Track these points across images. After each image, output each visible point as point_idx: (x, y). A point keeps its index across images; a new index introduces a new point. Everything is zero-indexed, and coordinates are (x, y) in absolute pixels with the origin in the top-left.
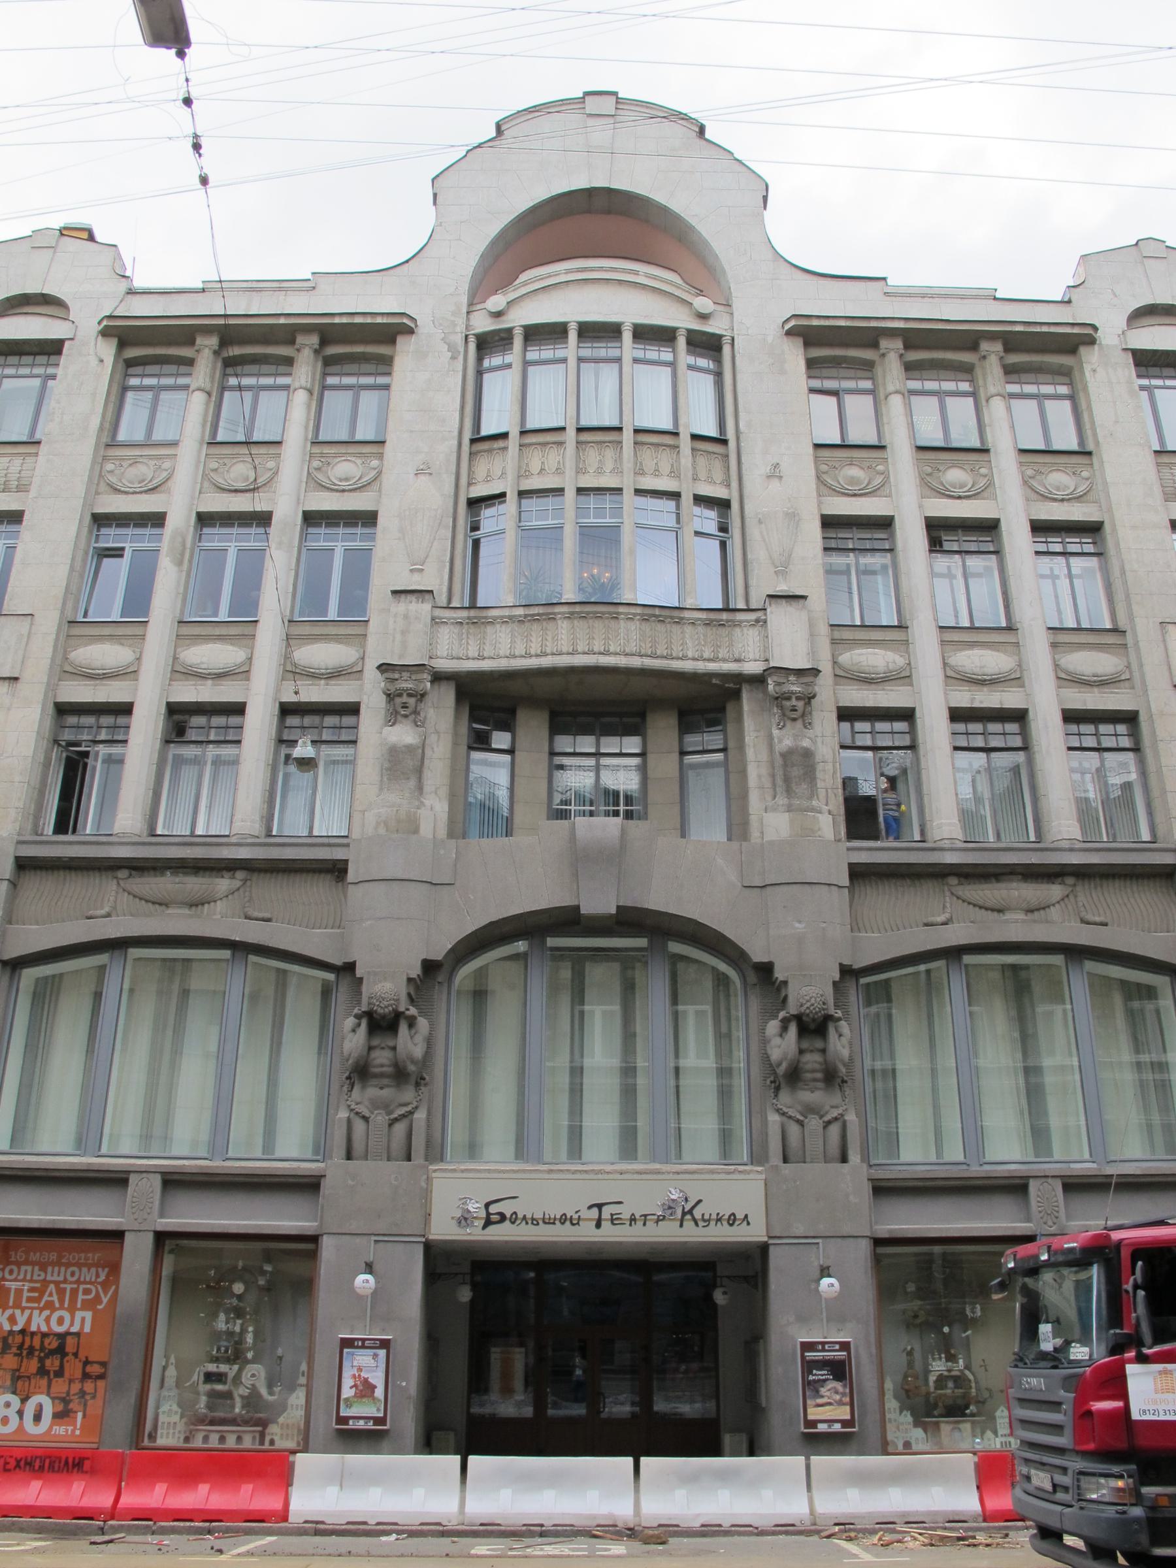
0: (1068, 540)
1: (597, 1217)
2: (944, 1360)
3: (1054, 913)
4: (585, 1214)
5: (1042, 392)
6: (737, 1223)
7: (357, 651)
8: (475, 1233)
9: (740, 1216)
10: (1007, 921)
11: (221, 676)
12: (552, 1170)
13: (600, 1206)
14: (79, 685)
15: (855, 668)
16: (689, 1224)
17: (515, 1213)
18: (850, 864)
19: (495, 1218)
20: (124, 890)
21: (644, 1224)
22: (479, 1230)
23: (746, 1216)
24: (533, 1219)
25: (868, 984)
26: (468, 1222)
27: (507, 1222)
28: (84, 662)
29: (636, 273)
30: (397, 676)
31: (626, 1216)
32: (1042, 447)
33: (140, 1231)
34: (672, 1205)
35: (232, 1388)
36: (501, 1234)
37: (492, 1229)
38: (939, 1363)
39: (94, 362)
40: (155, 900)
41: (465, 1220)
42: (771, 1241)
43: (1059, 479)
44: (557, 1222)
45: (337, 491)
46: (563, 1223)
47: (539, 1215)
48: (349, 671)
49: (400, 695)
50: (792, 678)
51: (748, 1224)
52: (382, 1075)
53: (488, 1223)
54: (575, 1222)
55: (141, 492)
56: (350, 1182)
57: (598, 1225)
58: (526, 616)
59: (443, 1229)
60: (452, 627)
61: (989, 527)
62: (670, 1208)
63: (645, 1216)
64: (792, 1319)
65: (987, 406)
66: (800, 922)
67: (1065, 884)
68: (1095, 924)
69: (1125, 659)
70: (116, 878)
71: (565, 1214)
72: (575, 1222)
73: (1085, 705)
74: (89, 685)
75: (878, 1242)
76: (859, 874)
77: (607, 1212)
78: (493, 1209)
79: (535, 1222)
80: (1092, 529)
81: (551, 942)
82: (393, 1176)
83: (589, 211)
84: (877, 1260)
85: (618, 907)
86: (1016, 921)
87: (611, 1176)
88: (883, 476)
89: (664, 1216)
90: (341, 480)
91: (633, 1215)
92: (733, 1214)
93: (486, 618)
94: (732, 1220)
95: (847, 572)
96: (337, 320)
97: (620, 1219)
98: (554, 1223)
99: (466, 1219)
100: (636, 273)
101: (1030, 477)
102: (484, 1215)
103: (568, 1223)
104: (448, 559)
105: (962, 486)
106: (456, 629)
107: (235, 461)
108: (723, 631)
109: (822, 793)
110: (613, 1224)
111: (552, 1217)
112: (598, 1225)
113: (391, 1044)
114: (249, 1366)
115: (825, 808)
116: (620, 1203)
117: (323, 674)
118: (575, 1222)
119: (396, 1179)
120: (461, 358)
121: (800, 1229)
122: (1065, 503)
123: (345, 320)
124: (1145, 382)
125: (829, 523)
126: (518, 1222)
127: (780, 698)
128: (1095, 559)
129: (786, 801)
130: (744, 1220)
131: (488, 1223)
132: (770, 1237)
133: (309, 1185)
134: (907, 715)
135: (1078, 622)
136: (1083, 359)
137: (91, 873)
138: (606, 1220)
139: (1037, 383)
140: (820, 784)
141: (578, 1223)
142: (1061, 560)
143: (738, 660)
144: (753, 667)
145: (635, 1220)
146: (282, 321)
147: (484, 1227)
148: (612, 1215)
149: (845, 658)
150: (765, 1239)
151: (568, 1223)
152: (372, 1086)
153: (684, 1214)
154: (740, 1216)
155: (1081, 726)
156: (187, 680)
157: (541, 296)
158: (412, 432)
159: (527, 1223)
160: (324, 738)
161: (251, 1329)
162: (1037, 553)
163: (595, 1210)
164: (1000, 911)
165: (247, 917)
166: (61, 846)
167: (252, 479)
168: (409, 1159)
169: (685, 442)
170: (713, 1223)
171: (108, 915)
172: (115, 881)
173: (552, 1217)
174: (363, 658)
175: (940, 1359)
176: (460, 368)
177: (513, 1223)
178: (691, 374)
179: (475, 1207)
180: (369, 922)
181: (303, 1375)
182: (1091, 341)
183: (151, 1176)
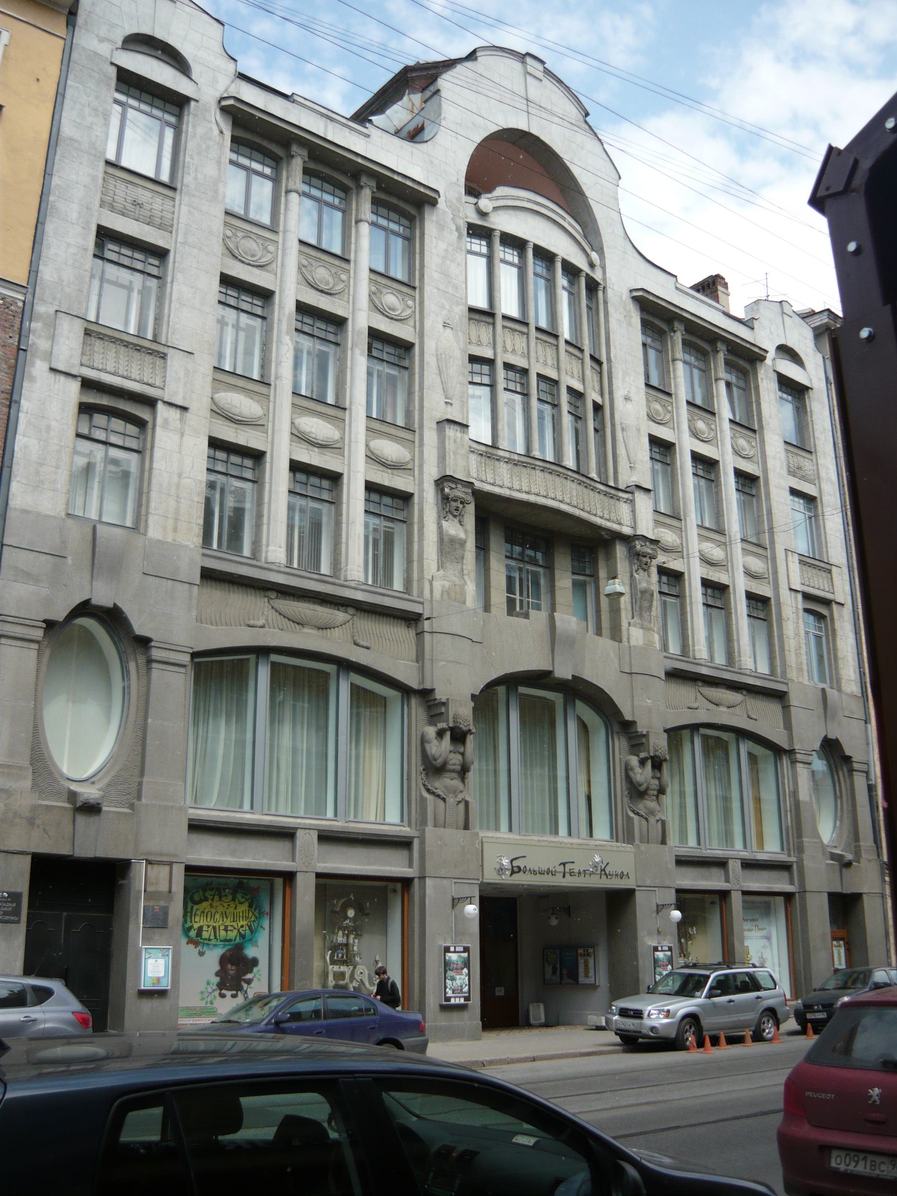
0: (243, 297)
3: (737, 710)
5: (239, 161)
8: (506, 879)
9: (625, 873)
11: (323, 446)
13: (564, 864)
14: (224, 425)
16: (604, 877)
18: (202, 567)
19: (516, 869)
20: (272, 608)
24: (534, 871)
25: (199, 663)
27: (522, 872)
30: (454, 486)
31: (576, 871)
32: (151, 174)
36: (521, 879)
37: (515, 876)
39: (216, 132)
40: (291, 618)
43: (322, 274)
45: (387, 317)
47: (536, 869)
49: (455, 501)
50: (648, 543)
52: (453, 771)
53: (513, 872)
55: (253, 266)
57: (564, 876)
59: (491, 876)
60: (476, 456)
61: (265, 295)
62: (596, 867)
63: (584, 871)
64: (645, 933)
66: (649, 699)
67: (346, 612)
68: (363, 647)
73: (751, 588)
74: (233, 428)
75: (319, 875)
76: (209, 576)
77: (568, 867)
78: (515, 863)
79: (534, 872)
80: (161, 254)
81: (522, 690)
83: (514, 143)
85: (573, 676)
88: (344, 284)
90: (390, 309)
93: (496, 455)
94: (622, 876)
95: (129, 288)
96: (396, 177)
99: (502, 870)
100: (564, 219)
101: (304, 266)
102: (510, 867)
105: (253, 256)
106: (479, 458)
108: (612, 501)
113: (462, 750)
116: (573, 862)
117: (389, 465)
121: (648, 883)
122: (745, 460)
123: (400, 179)
124: (122, 98)
125: (104, 235)
127: (638, 555)
128: (259, 320)
129: (638, 621)
131: (513, 872)
133: (404, 844)
134: (335, 478)
135: (235, 369)
136: (426, 216)
137: (249, 590)
139: (251, 159)
142: (233, 312)
143: (620, 524)
144: (627, 530)
146: (360, 160)
147: (511, 875)
149: (374, 444)
150: (635, 887)
152: (446, 777)
155: (244, 460)
156: (300, 443)
157: (511, 212)
160: (217, 469)
162: (220, 302)
163: (562, 866)
164: (717, 705)
165: (356, 644)
166: (234, 564)
167: (331, 286)
169: (499, 322)
171: (263, 627)
172: (266, 599)
178: (502, 265)
180: (442, 663)
182: (433, 203)
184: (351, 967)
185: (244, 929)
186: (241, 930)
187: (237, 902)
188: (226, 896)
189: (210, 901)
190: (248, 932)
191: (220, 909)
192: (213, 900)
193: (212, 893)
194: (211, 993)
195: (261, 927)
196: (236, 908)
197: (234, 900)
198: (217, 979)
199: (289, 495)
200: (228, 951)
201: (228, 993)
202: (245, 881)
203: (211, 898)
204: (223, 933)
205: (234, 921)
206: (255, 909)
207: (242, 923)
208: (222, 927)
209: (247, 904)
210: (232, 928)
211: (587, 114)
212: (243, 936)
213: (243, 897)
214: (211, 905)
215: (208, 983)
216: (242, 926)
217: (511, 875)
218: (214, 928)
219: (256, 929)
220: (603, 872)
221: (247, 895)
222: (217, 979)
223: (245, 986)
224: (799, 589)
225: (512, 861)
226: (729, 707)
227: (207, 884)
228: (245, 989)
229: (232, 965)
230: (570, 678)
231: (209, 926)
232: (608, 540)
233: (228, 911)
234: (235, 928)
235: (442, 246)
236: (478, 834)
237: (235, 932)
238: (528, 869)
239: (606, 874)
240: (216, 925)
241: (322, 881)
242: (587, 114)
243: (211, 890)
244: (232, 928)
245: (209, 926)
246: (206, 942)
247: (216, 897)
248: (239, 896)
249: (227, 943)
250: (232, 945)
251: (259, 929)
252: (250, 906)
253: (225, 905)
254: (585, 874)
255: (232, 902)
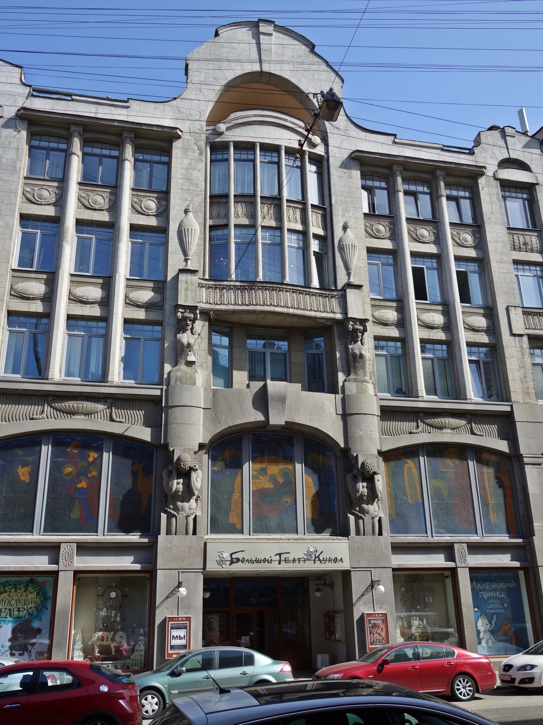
1: (279, 559)
2: (418, 620)
4: (274, 558)
6: (338, 561)
7: (160, 296)
8: (227, 568)
9: (339, 558)
10: (444, 433)
12: (259, 539)
13: (280, 555)
15: (381, 318)
16: (318, 562)
17: (244, 558)
21: (299, 562)
22: (228, 566)
23: (342, 558)
26: (224, 562)
27: (240, 562)
28: (22, 290)
29: (286, 120)
31: (291, 559)
33: (66, 571)
34: (311, 554)
35: (111, 643)
36: (238, 567)
38: (416, 622)
41: (221, 562)
42: (352, 570)
44: (262, 562)
46: (264, 562)
48: (157, 305)
51: (342, 562)
54: (270, 562)
55: (46, 205)
56: (169, 545)
57: (280, 563)
58: (241, 286)
62: (310, 555)
63: (299, 559)
65: (437, 201)
69: (492, 321)
70: (47, 400)
71: (265, 558)
72: (270, 562)
73: (475, 339)
77: (283, 557)
78: (234, 556)
79: (252, 562)
82: (188, 542)
84: (394, 576)
86: (448, 433)
87: (284, 541)
89: (307, 559)
91: (294, 558)
92: (336, 558)
94: (336, 560)
97: (289, 560)
98: (261, 562)
99: (222, 561)
100: (286, 120)
102: (230, 559)
103: (266, 562)
104: (203, 255)
107: (95, 193)
109: (368, 374)
110: (286, 562)
111: (260, 559)
112: (280, 563)
114: (118, 632)
115: (370, 381)
118: (270, 562)
119: (190, 543)
120: (204, 155)
126: (245, 562)
130: (340, 560)
131: (232, 562)
132: (351, 568)
138: (283, 560)
140: (368, 370)
141: (271, 563)
145: (295, 560)
147: (230, 565)
148: (285, 558)
150: (350, 569)
151: (266, 562)
153: (315, 557)
154: (339, 558)
158: (182, 189)
159: (249, 562)
161: (119, 615)
163: (278, 556)
168: (195, 534)
170: (328, 562)
173: (260, 559)
174: (163, 300)
175: (416, 620)
176: (204, 159)
177: (243, 562)
179: (226, 556)
181: (141, 635)
183: (71, 544)
184: (112, 633)
185: (32, 609)
186: (29, 611)
187: (28, 592)
188: (20, 589)
189: (8, 593)
190: (35, 612)
191: (15, 597)
192: (10, 592)
193: (10, 587)
194: (4, 653)
195: (45, 608)
196: (27, 596)
197: (26, 591)
198: (9, 644)
199: (369, 258)
200: (19, 624)
201: (17, 653)
202: (35, 578)
203: (9, 590)
204: (16, 613)
205: (25, 605)
206: (42, 595)
207: (31, 606)
208: (16, 609)
209: (35, 593)
210: (23, 610)
211: (314, 46)
212: (31, 615)
213: (32, 589)
214: (9, 595)
215: (3, 647)
216: (31, 608)
217: (230, 565)
218: (10, 610)
219: (41, 610)
220: (317, 559)
221: (36, 587)
222: (9, 644)
223: (30, 647)
224: (522, 333)
225: (231, 555)
226: (453, 429)
227: (7, 582)
228: (29, 649)
229: (21, 634)
230: (284, 424)
231: (6, 609)
232: (331, 325)
233: (21, 599)
234: (25, 610)
235: (186, 162)
236: (203, 537)
237: (25, 612)
238: (246, 559)
239: (319, 560)
240: (12, 608)
241: (397, 573)
242: (314, 46)
243: (9, 585)
244: (23, 610)
245: (6, 609)
246: (3, 619)
247: (13, 590)
248: (30, 588)
249: (18, 620)
250: (23, 620)
251: (43, 609)
252: (38, 594)
253: (19, 595)
254: (299, 561)
255: (24, 593)
